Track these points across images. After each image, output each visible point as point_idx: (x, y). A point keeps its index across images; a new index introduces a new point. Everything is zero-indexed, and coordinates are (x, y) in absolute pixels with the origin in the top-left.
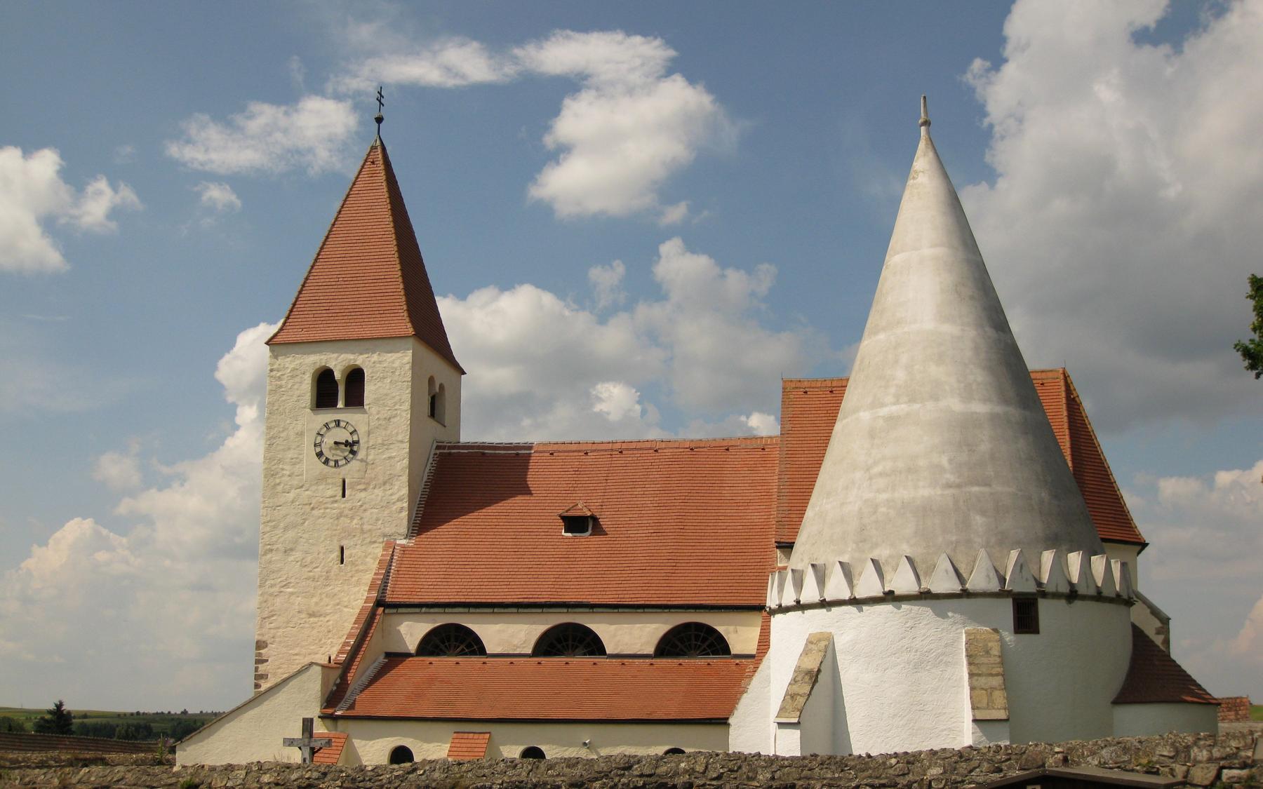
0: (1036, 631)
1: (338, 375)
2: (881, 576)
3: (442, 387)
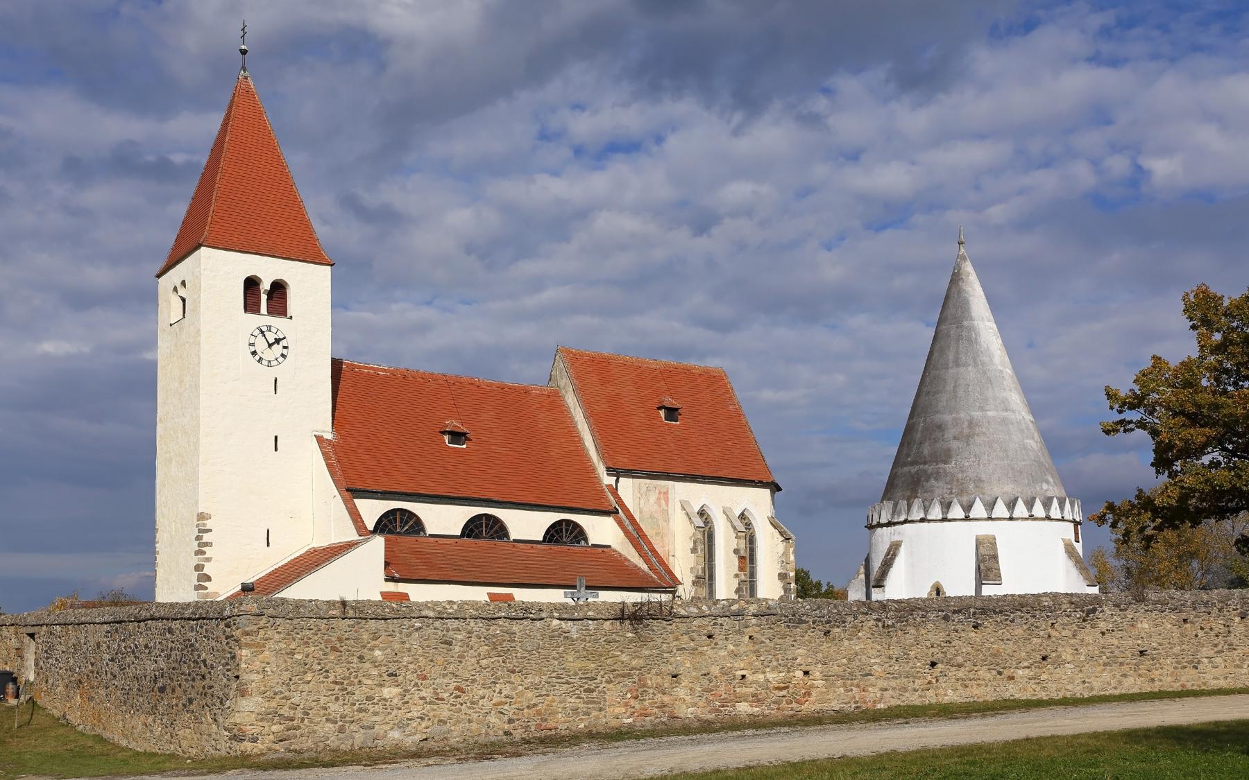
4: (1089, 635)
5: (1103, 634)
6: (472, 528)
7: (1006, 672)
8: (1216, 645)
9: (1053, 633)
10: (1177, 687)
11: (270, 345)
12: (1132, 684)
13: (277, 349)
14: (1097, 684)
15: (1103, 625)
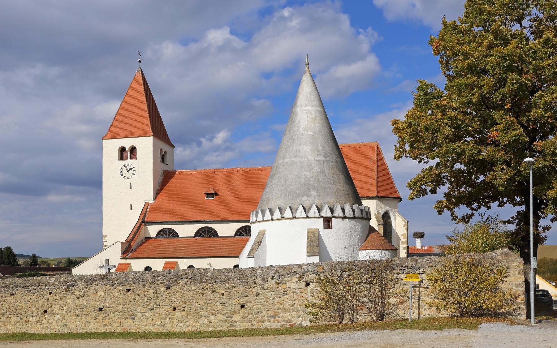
0: (331, 229)
1: (127, 149)
2: (319, 213)
3: (165, 152)
4: (70, 299)
5: (78, 298)
6: (199, 233)
7: (25, 319)
8: (148, 305)
9: (50, 298)
10: (119, 330)
11: (128, 171)
12: (94, 327)
13: (131, 172)
14: (71, 326)
15: (77, 293)
